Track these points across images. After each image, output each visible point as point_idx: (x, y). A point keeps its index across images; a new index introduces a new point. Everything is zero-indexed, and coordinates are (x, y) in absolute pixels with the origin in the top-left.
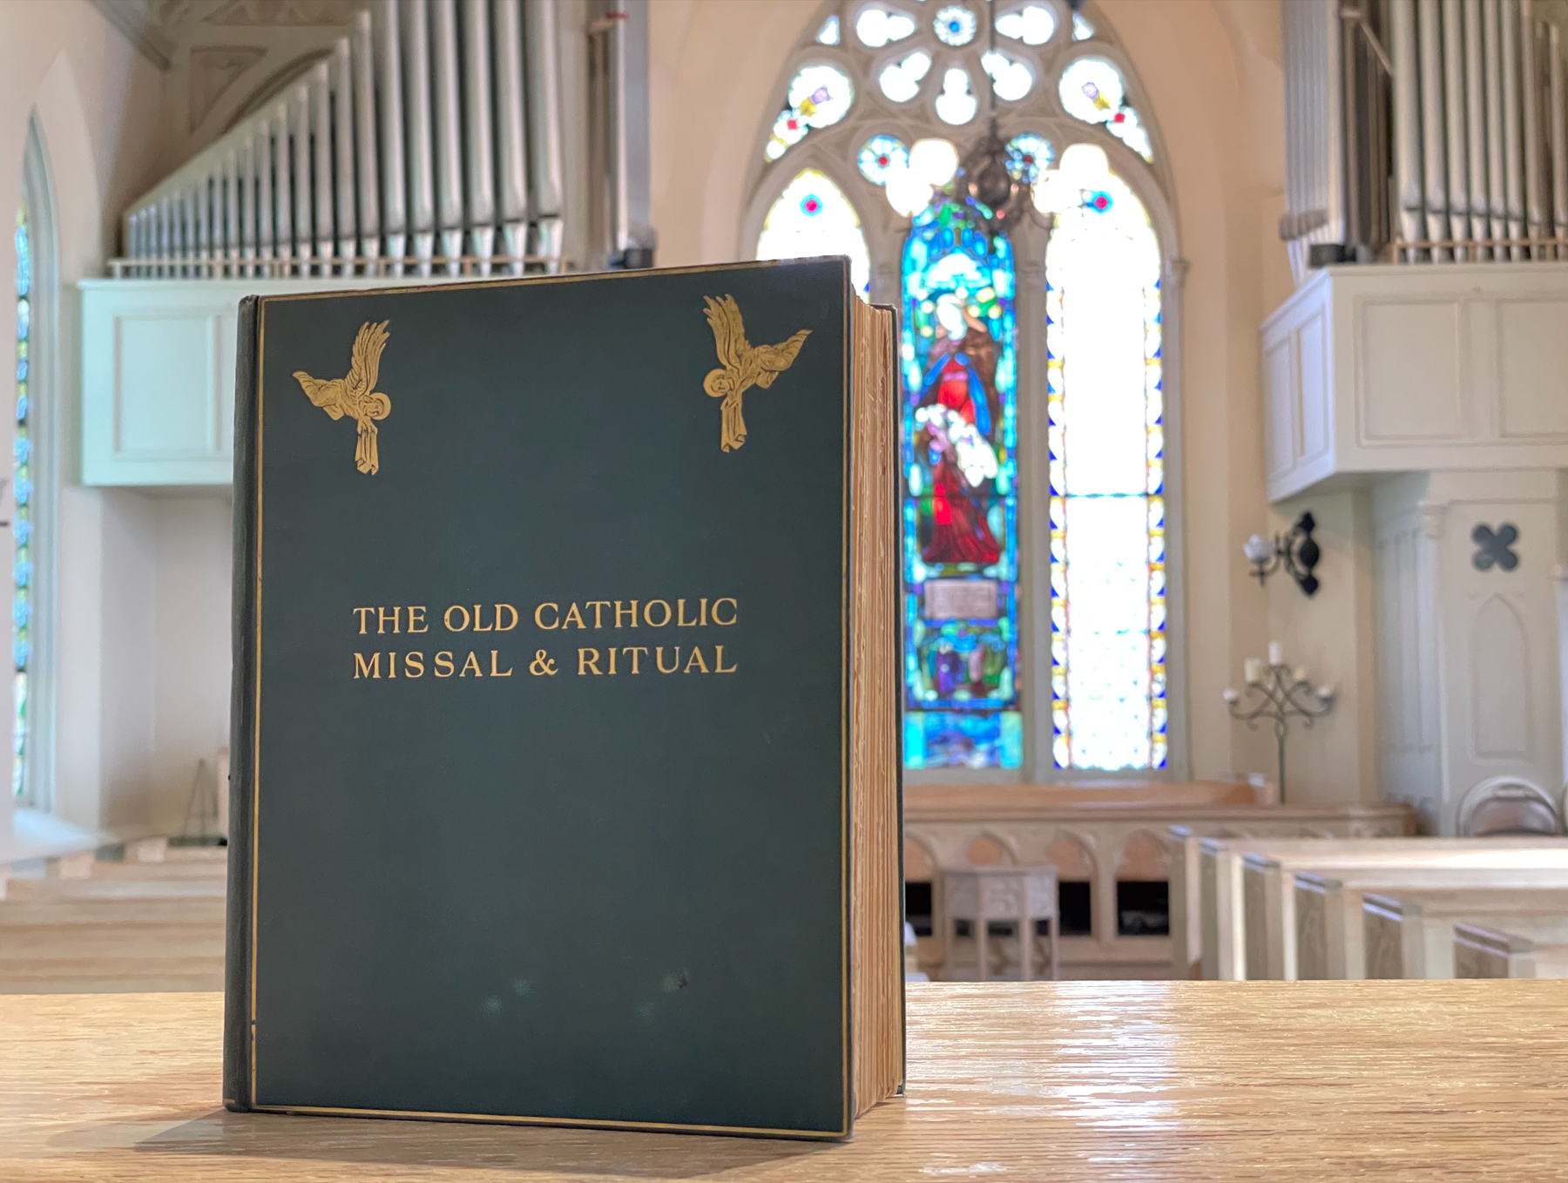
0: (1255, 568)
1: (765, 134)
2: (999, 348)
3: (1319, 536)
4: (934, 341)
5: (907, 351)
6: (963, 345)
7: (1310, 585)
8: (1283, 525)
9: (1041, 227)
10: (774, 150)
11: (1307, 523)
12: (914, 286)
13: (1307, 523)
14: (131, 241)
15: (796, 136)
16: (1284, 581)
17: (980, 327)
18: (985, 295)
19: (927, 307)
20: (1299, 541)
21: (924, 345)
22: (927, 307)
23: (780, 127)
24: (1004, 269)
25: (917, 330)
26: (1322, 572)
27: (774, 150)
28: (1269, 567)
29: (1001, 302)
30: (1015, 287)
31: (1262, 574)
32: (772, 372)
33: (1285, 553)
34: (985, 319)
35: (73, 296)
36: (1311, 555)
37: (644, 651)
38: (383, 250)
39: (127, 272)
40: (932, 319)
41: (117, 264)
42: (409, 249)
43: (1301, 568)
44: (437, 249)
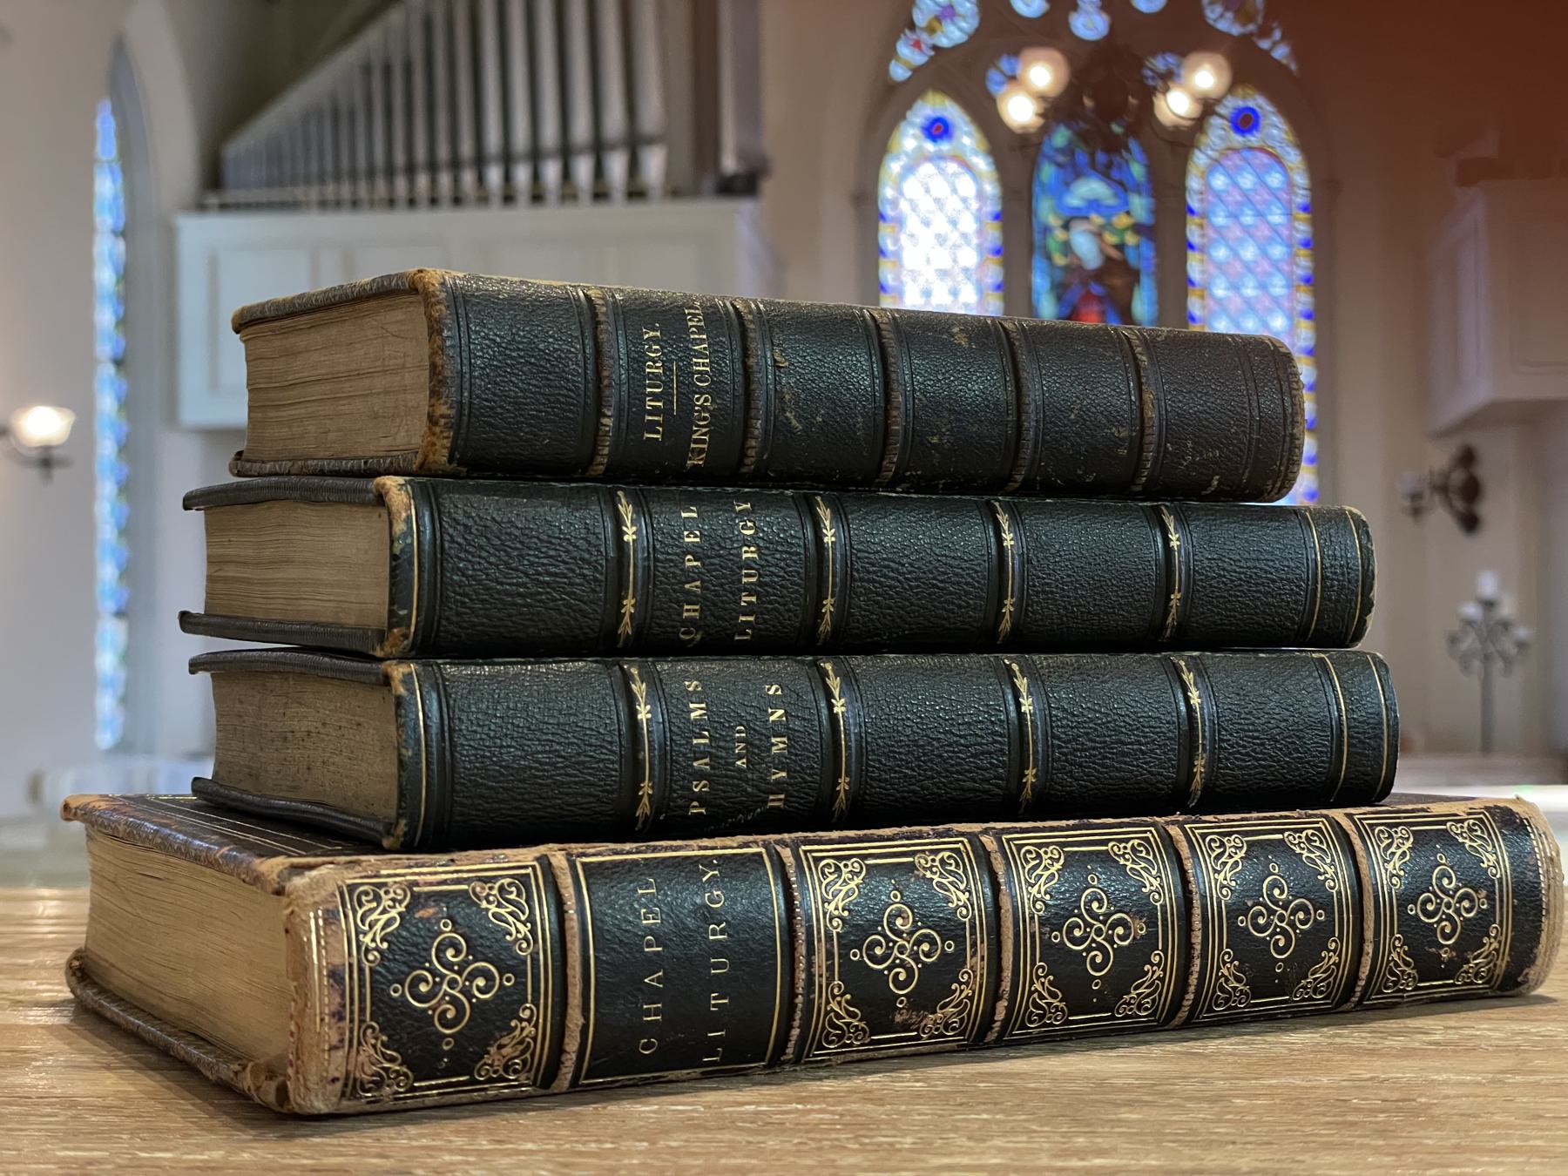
0: (1407, 503)
1: (890, 53)
2: (1134, 276)
3: (1484, 471)
4: (1067, 268)
5: (1040, 281)
6: (1099, 275)
7: (1470, 523)
8: (1440, 458)
9: (918, 216)
10: (899, 72)
11: (1467, 458)
12: (1046, 212)
13: (1467, 458)
14: (230, 173)
15: (919, 59)
16: (1441, 519)
17: (1114, 253)
18: (1122, 221)
19: (1060, 235)
20: (1458, 477)
21: (1059, 276)
22: (1060, 235)
23: (904, 50)
24: (1139, 193)
25: (1049, 258)
26: (1487, 509)
27: (899, 72)
28: (1424, 502)
29: (1137, 228)
30: (1156, 212)
31: (1417, 512)
32: (984, 857)
33: (1443, 489)
34: (1120, 247)
35: (170, 236)
36: (1472, 490)
37: (892, 209)
38: (481, 179)
39: (224, 207)
40: (1067, 248)
41: (213, 200)
42: (508, 178)
43: (1459, 505)
44: (536, 176)
